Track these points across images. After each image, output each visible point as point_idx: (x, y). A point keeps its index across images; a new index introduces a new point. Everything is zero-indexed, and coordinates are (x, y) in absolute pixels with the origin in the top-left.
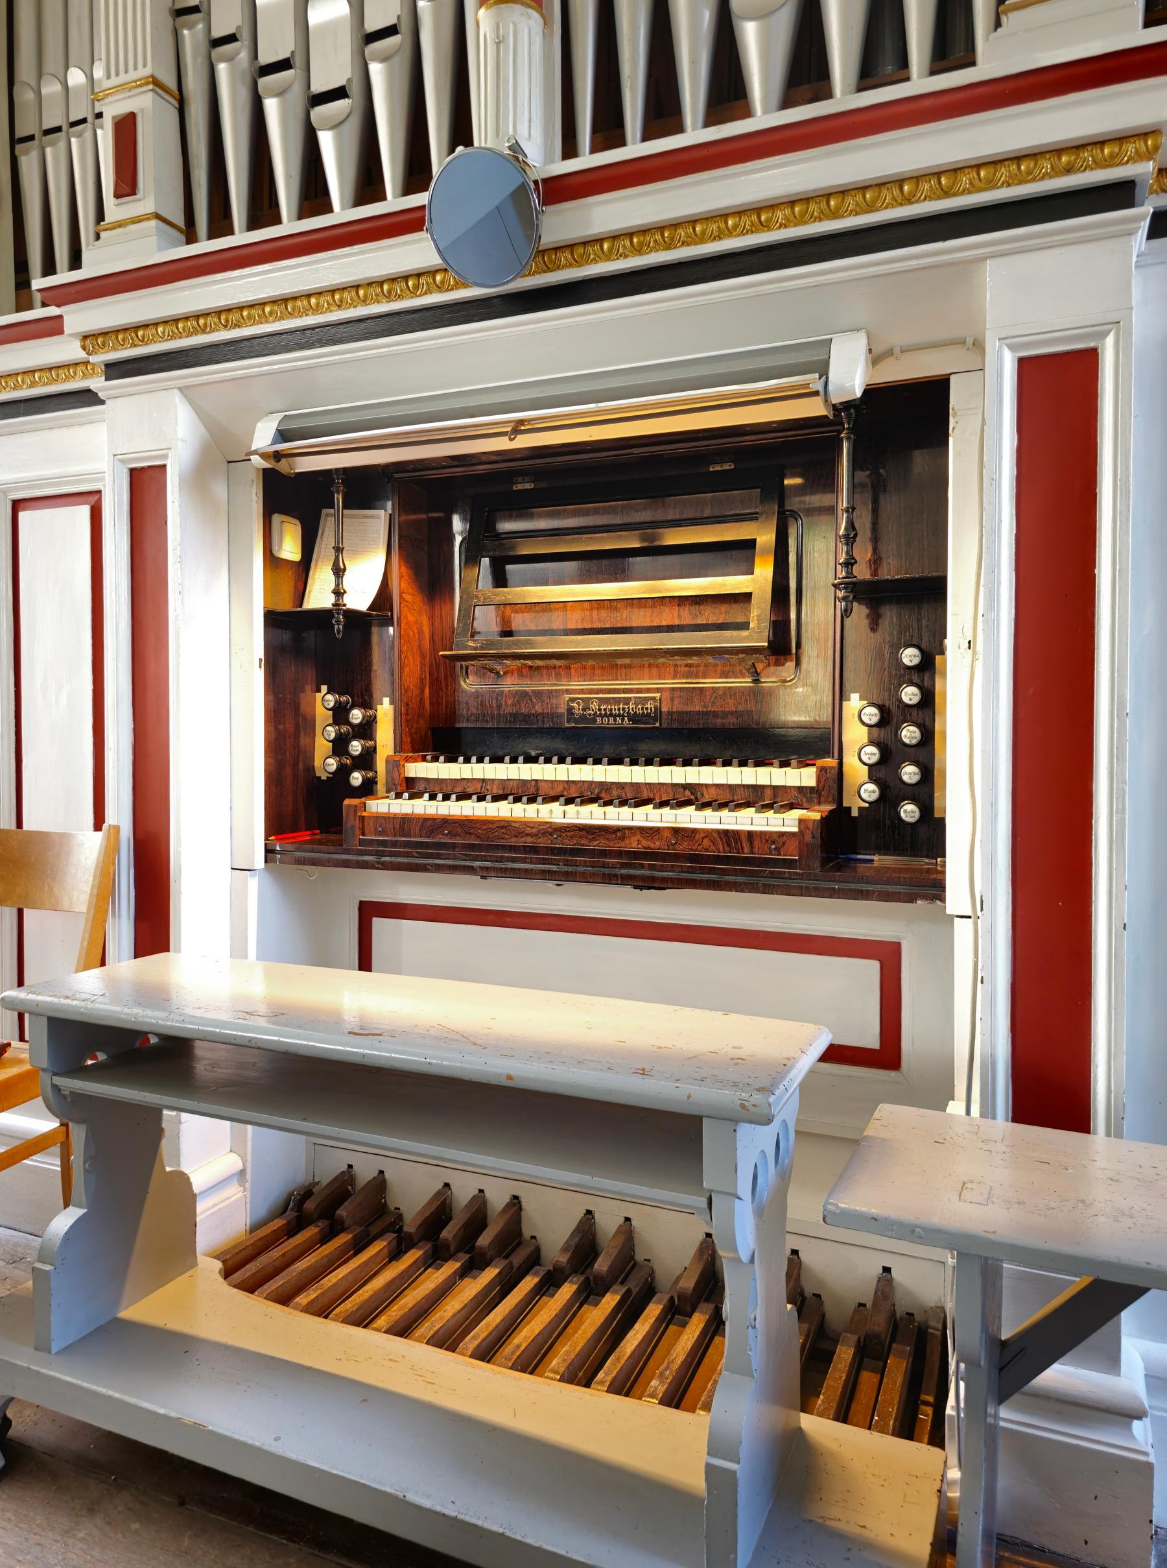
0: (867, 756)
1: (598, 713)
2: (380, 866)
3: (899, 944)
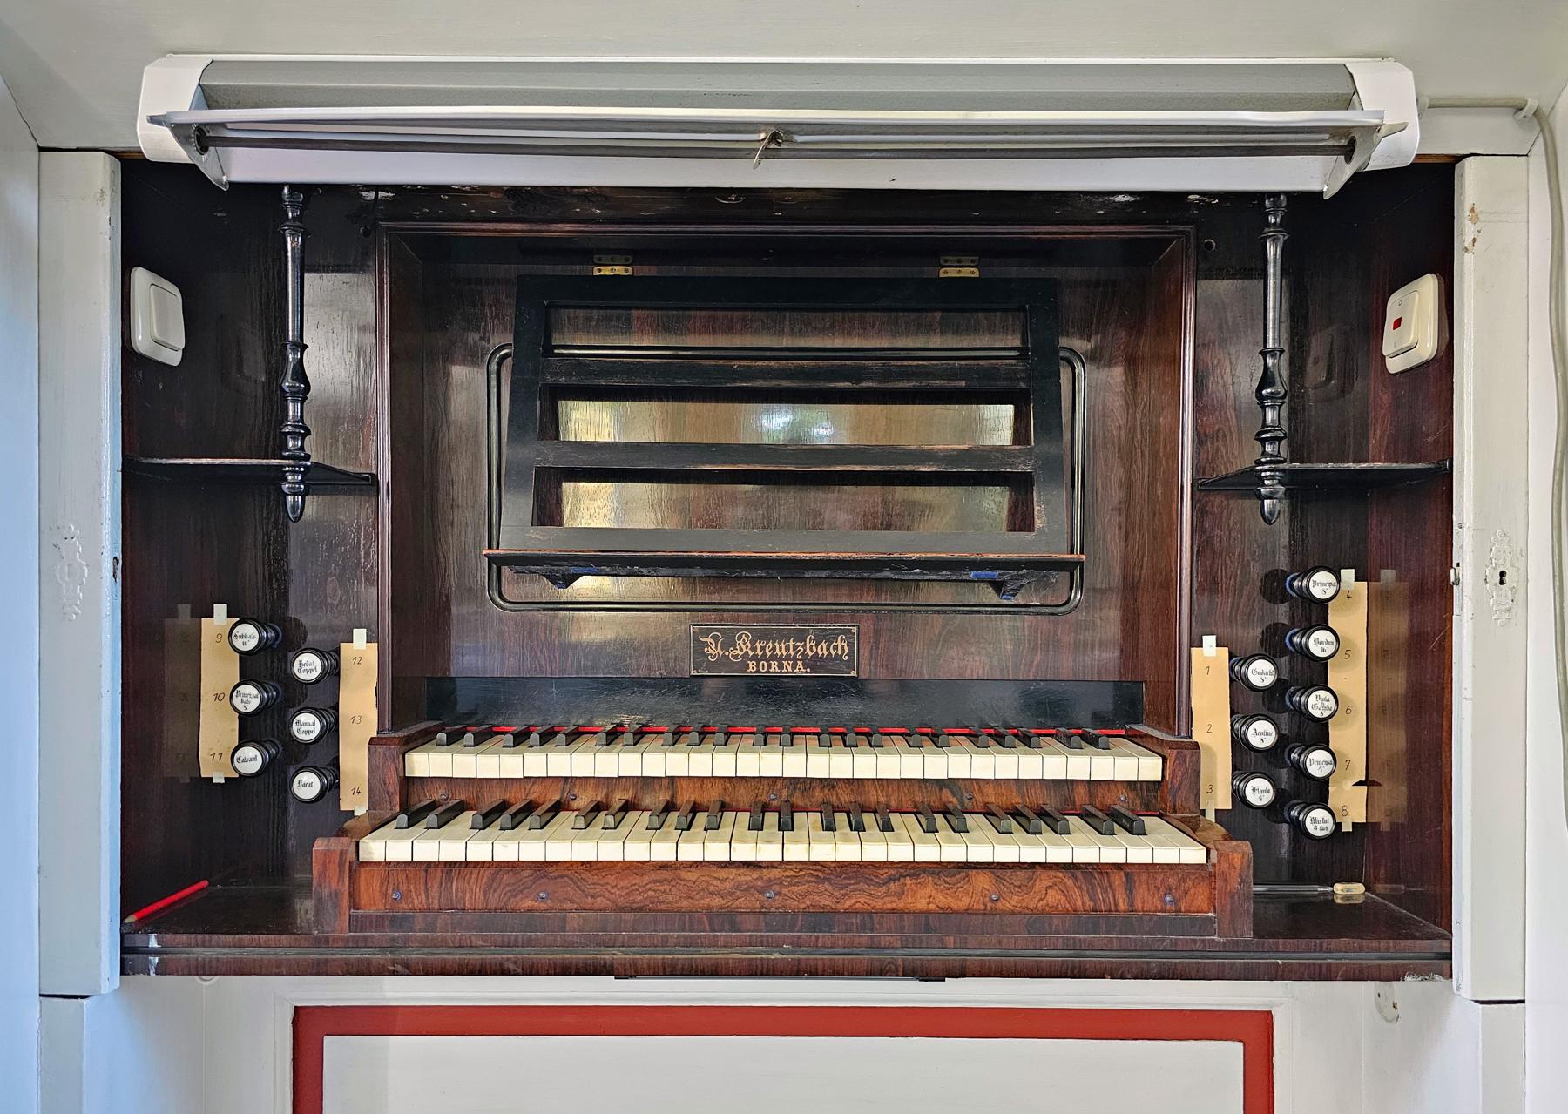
0: (1260, 737)
1: (751, 654)
2: (399, 968)
3: (1269, 1015)
